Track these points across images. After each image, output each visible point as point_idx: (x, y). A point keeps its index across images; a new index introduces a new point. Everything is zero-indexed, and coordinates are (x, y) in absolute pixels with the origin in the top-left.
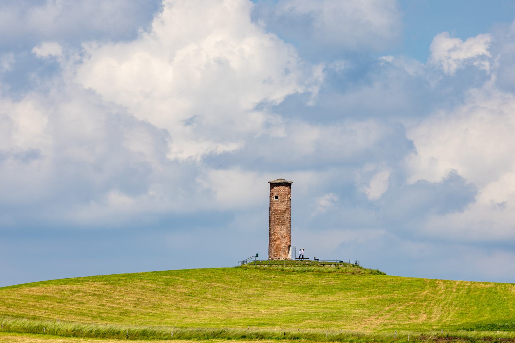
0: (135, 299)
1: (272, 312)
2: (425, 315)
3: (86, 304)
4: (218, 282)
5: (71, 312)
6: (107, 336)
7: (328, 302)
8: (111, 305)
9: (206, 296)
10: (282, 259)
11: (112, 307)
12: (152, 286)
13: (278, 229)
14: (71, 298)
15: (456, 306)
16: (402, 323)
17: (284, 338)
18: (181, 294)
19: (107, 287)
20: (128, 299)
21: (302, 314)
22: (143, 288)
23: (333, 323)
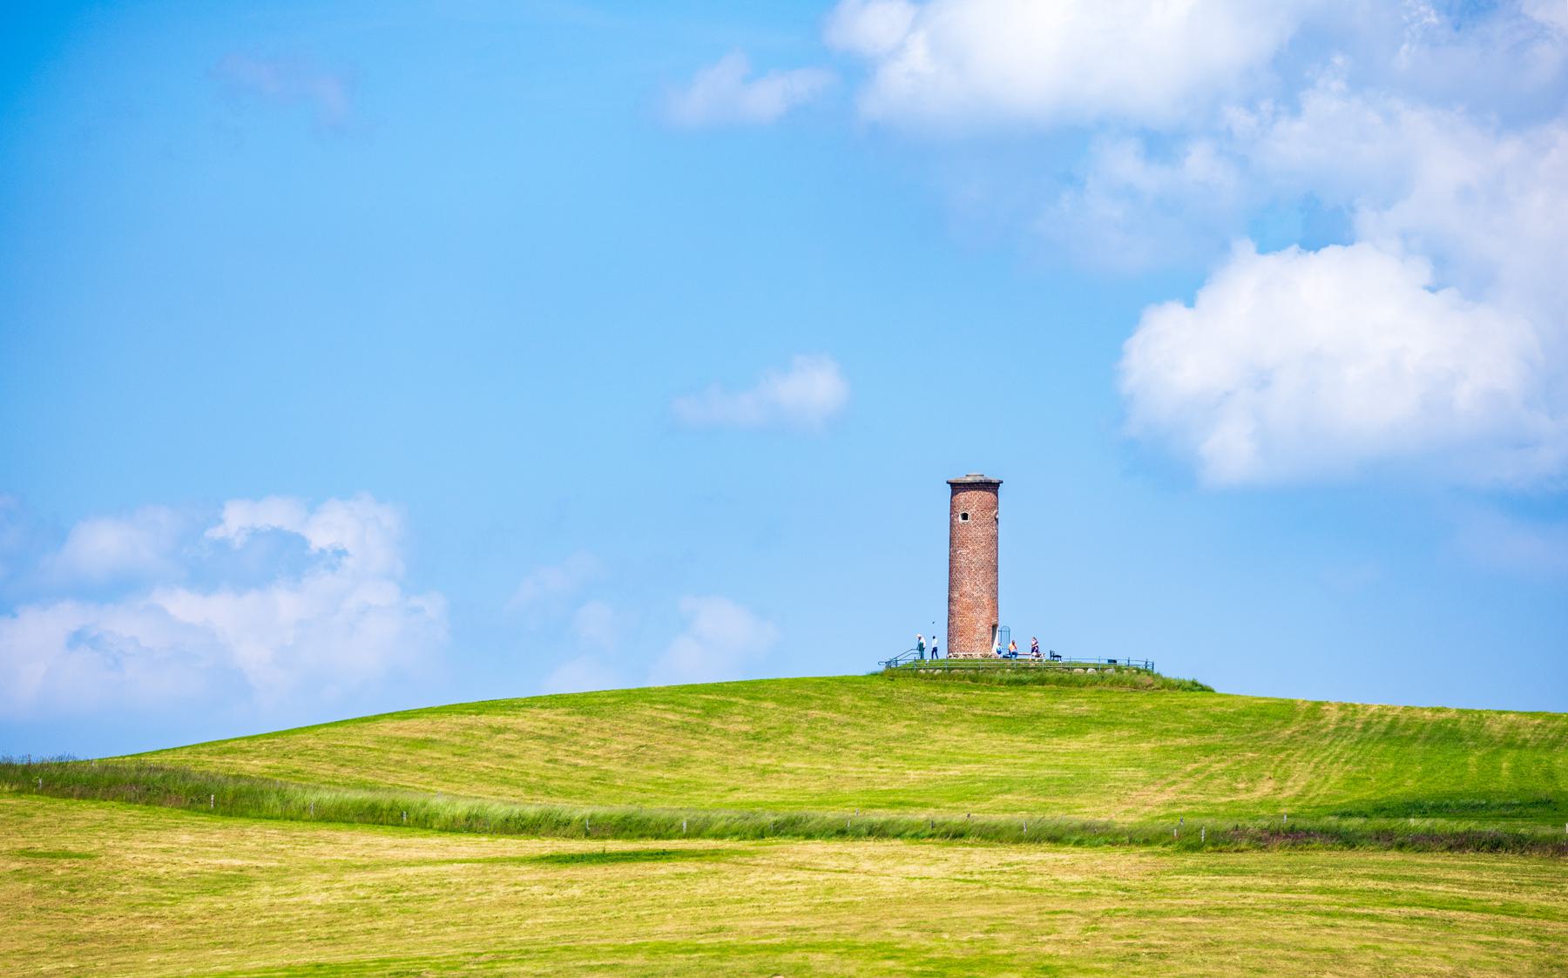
0: (631, 747)
1: (933, 775)
2: (1271, 783)
3: (519, 757)
4: (824, 708)
5: (480, 776)
6: (543, 830)
7: (1064, 755)
8: (574, 761)
9: (791, 738)
10: (977, 655)
11: (576, 765)
12: (674, 718)
13: (967, 588)
14: (486, 744)
15: (1347, 762)
16: (1213, 801)
17: (931, 836)
18: (737, 735)
19: (572, 719)
20: (615, 746)
21: (996, 781)
22: (653, 722)
23: (1059, 800)
